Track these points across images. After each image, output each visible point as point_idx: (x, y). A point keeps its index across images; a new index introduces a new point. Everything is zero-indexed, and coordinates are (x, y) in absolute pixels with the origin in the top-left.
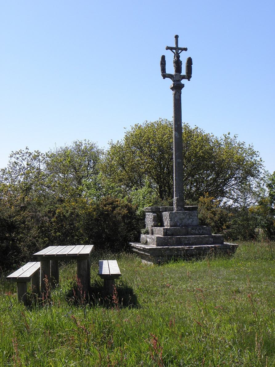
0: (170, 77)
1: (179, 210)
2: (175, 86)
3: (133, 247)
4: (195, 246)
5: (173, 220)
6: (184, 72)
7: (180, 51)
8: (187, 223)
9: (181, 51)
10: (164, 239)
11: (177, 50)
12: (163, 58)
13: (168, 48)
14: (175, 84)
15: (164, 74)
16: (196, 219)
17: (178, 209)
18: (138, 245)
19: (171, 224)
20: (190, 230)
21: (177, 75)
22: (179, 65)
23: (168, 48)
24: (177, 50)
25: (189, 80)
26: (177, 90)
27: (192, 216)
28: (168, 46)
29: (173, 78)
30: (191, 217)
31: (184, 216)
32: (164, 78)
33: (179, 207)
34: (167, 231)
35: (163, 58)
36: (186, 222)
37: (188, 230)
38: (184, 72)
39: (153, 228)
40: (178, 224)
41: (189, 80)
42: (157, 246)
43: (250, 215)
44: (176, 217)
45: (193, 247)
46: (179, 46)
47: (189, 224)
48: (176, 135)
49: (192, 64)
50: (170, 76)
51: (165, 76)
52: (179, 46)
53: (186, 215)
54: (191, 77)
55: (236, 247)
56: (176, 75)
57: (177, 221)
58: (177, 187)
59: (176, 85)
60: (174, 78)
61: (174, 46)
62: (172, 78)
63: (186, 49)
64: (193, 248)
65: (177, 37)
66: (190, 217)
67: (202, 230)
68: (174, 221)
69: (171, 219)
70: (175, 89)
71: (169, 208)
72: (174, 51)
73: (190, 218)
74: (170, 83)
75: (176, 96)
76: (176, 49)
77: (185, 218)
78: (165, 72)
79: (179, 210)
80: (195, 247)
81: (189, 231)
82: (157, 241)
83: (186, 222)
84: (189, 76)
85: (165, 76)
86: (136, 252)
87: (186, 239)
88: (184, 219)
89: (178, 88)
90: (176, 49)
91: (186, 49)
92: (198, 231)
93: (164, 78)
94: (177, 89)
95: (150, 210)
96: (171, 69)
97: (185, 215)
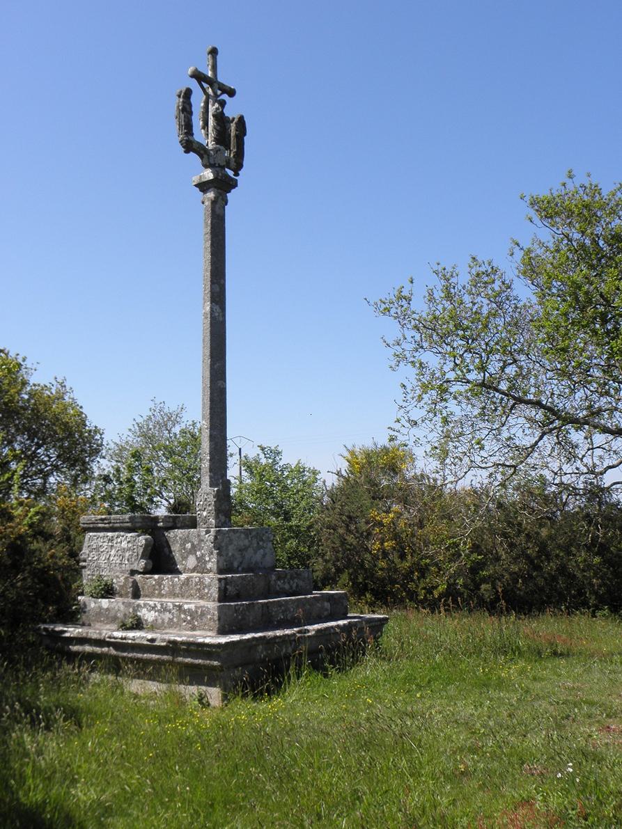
0: (202, 152)
1: (220, 525)
3: (72, 640)
4: (316, 627)
5: (224, 553)
8: (253, 561)
10: (236, 611)
16: (271, 549)
17: (218, 521)
18: (72, 631)
19: (219, 564)
20: (275, 581)
22: (225, 126)
27: (262, 540)
28: (199, 70)
29: (209, 158)
30: (261, 543)
31: (246, 542)
33: (220, 516)
34: (228, 587)
35: (188, 93)
36: (252, 557)
37: (270, 581)
39: (138, 577)
40: (236, 564)
42: (222, 632)
44: (232, 544)
45: (308, 631)
47: (256, 563)
48: (217, 314)
49: (245, 134)
53: (252, 538)
55: (383, 621)
57: (233, 555)
58: (216, 457)
62: (205, 156)
64: (313, 633)
65: (214, 52)
66: (258, 543)
67: (296, 580)
68: (227, 554)
69: (218, 549)
70: (215, 187)
71: (181, 518)
73: (259, 547)
77: (249, 547)
79: (220, 525)
80: (319, 631)
81: (272, 582)
82: (219, 619)
83: (252, 557)
86: (90, 656)
87: (280, 606)
88: (246, 548)
89: (222, 186)
92: (289, 583)
93: (187, 152)
95: (127, 522)
97: (250, 539)
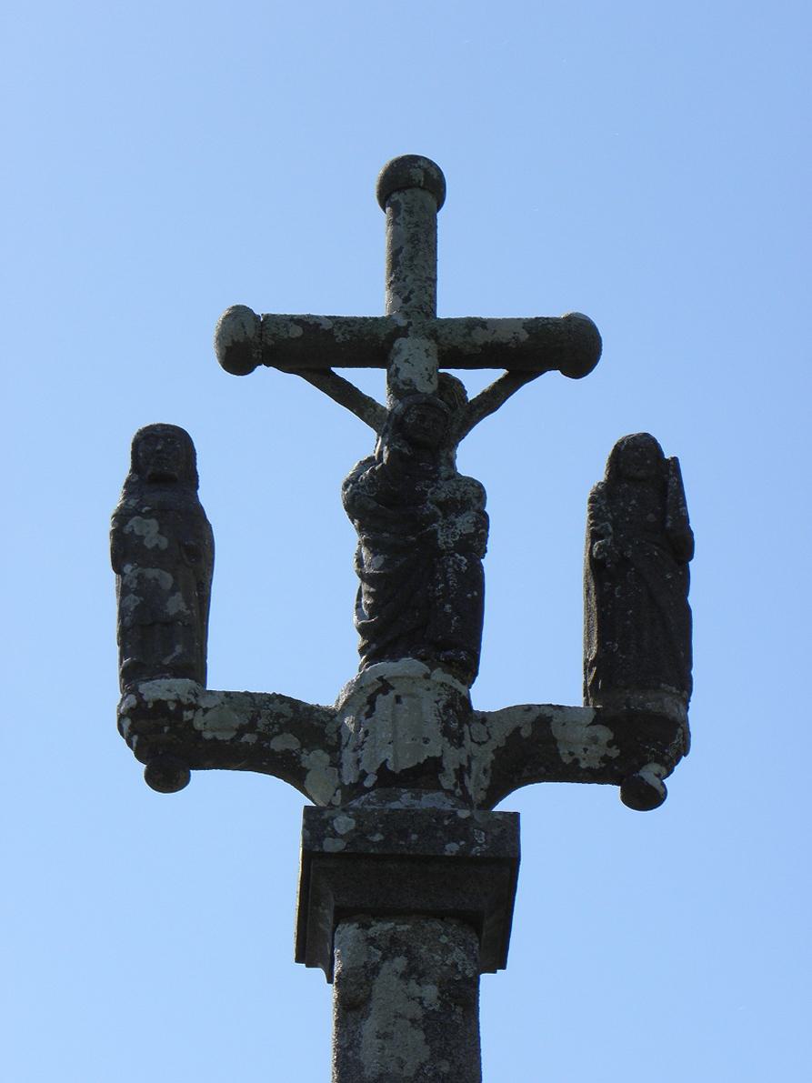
2: (331, 845)
6: (533, 647)
7: (476, 381)
9: (500, 373)
11: (419, 378)
12: (163, 463)
13: (250, 343)
14: (343, 824)
15: (160, 689)
21: (385, 686)
23: (250, 343)
24: (419, 378)
25: (644, 797)
26: (380, 928)
28: (260, 310)
32: (166, 776)
35: (163, 463)
38: (533, 647)
41: (644, 797)
43: (278, 321)
46: (453, 302)
49: (690, 556)
50: (269, 735)
51: (177, 729)
52: (453, 302)
54: (605, 504)
56: (366, 696)
59: (360, 834)
60: (348, 756)
61: (369, 297)
62: (316, 759)
63: (567, 346)
72: (372, 382)
74: (254, 822)
75: (370, 1026)
76: (400, 332)
78: (195, 667)
84: (634, 725)
85: (177, 729)
90: (400, 332)
91: (567, 346)
93: (166, 776)
94: (382, 914)
96: (288, 620)
